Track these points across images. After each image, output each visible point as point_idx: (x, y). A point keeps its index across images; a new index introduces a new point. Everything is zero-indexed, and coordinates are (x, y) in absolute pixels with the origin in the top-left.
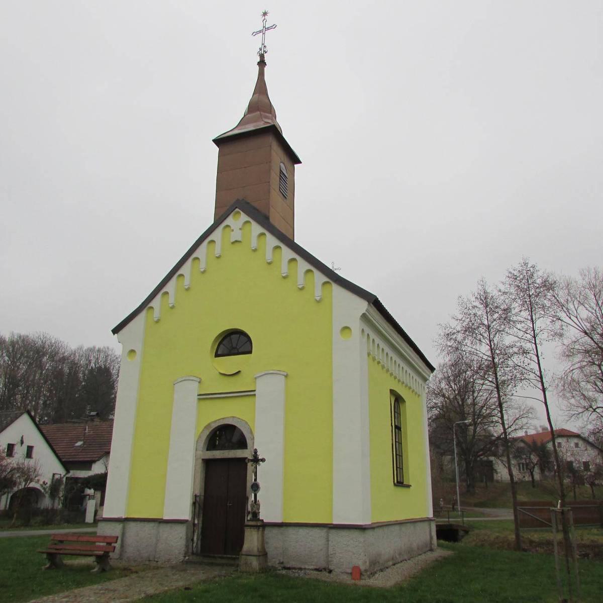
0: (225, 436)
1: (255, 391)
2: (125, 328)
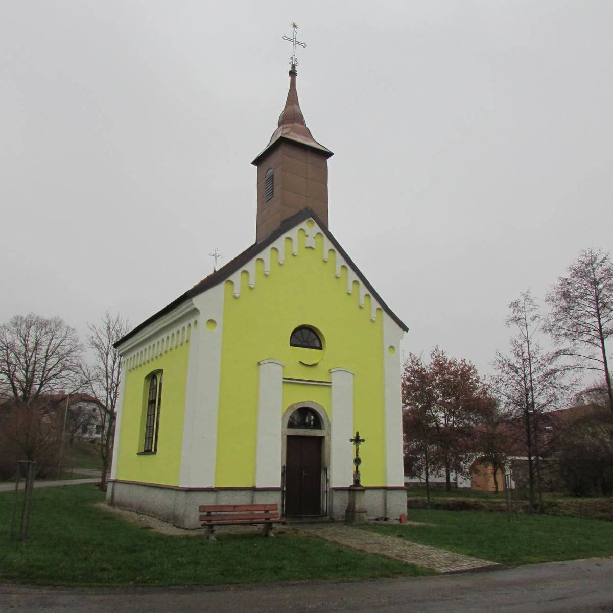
0: (306, 418)
1: (330, 383)
2: (204, 293)
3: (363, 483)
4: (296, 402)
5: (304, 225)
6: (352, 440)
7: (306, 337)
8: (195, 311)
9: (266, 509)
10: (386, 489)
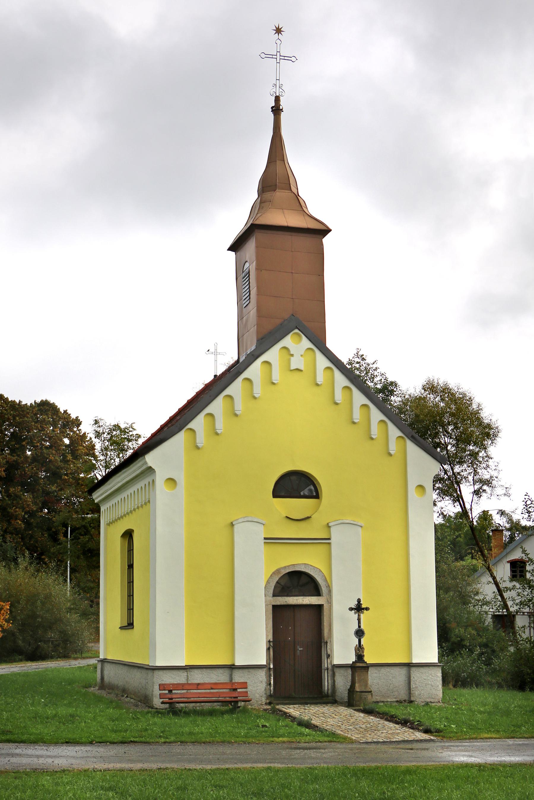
3: (369, 659)
4: (283, 566)
5: (288, 341)
6: (351, 609)
7: (295, 485)
8: (150, 470)
9: (234, 687)
10: (409, 665)
